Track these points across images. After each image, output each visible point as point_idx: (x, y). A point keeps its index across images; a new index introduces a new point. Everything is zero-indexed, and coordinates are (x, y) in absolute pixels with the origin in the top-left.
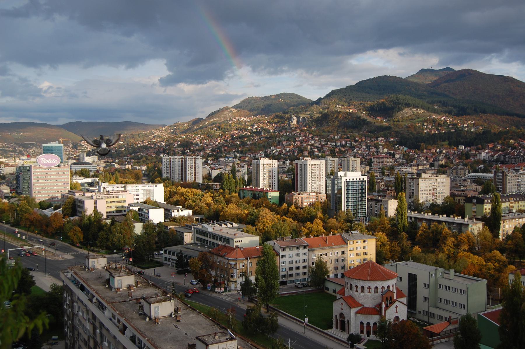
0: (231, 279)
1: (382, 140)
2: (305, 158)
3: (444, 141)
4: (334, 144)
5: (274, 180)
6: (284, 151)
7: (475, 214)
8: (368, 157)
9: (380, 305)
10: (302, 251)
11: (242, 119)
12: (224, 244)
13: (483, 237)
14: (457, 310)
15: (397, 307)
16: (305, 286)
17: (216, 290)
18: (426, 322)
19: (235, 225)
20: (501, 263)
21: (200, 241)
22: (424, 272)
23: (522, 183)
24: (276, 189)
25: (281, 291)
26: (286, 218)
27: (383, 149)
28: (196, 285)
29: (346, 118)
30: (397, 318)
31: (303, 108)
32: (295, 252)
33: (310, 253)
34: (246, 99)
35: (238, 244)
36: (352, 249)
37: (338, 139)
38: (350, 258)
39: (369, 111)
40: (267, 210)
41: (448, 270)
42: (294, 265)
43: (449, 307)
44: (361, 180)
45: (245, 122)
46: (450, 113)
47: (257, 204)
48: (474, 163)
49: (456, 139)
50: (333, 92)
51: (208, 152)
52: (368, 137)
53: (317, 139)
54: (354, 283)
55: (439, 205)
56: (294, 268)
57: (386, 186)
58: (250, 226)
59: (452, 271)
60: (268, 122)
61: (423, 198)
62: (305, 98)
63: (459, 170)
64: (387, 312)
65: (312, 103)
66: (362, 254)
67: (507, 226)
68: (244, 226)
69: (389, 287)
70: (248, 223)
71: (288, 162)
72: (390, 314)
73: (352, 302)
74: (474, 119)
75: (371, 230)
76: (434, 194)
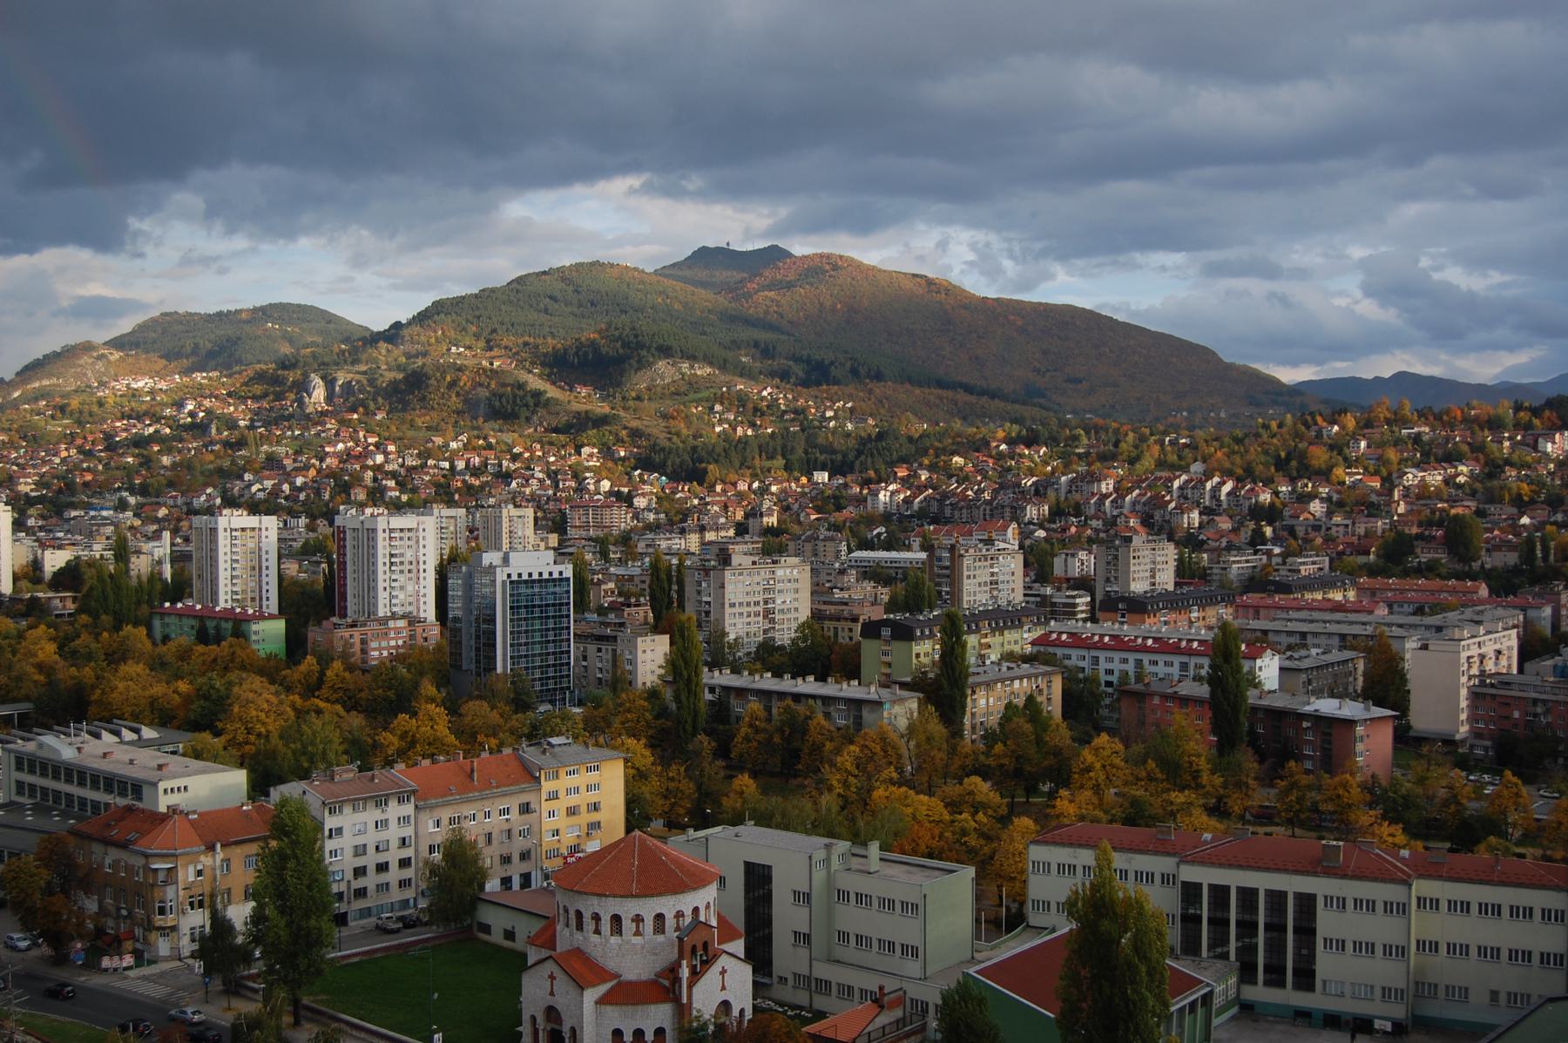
0: (159, 920)
1: (591, 455)
2: (368, 511)
3: (771, 457)
4: (446, 465)
5: (265, 580)
6: (286, 487)
7: (888, 671)
8: (551, 505)
9: (673, 970)
10: (395, 810)
11: (140, 384)
12: (122, 802)
13: (922, 737)
14: (894, 962)
15: (723, 972)
16: (409, 924)
17: (106, 962)
18: (801, 1008)
19: (148, 733)
20: (990, 812)
21: (32, 794)
22: (792, 856)
23: (1001, 578)
24: (274, 609)
25: (346, 947)
26: (322, 704)
27: (598, 481)
28: (28, 949)
29: (481, 385)
30: (726, 1005)
31: (343, 352)
32: (372, 815)
33: (424, 816)
34: (153, 320)
35: (173, 799)
36: (554, 796)
37: (459, 450)
38: (548, 824)
39: (551, 366)
40: (257, 682)
41: (865, 844)
42: (370, 860)
43: (872, 957)
44: (556, 575)
45: (152, 392)
46: (784, 376)
47: (215, 660)
48: (858, 523)
49: (806, 452)
50: (438, 308)
51: (27, 489)
52: (551, 443)
53: (391, 448)
54: (590, 906)
55: (782, 648)
56: (371, 869)
57: (620, 594)
58: (206, 736)
59: (874, 849)
60: (230, 395)
61: (739, 626)
62: (349, 323)
63: (821, 544)
64: (695, 990)
65: (374, 338)
66: (584, 808)
67: (983, 702)
68: (184, 740)
69: (696, 910)
70: (196, 727)
71: (303, 521)
72: (705, 998)
73: (583, 970)
74: (851, 397)
75: (598, 730)
76: (768, 614)
